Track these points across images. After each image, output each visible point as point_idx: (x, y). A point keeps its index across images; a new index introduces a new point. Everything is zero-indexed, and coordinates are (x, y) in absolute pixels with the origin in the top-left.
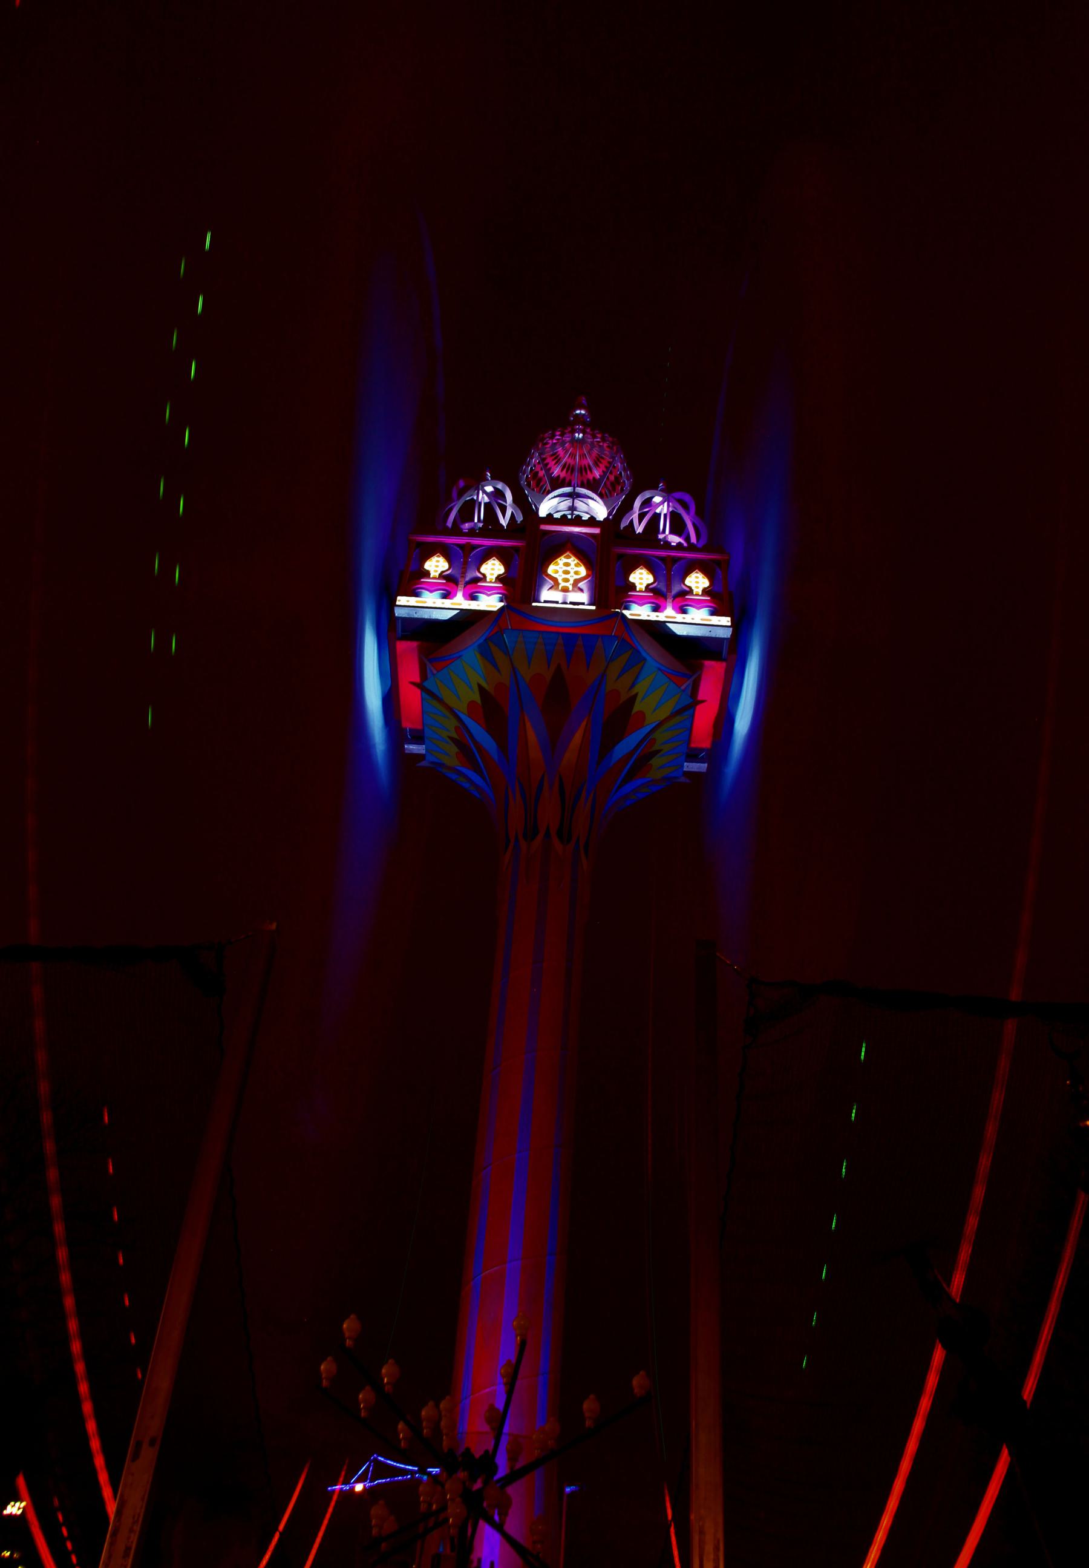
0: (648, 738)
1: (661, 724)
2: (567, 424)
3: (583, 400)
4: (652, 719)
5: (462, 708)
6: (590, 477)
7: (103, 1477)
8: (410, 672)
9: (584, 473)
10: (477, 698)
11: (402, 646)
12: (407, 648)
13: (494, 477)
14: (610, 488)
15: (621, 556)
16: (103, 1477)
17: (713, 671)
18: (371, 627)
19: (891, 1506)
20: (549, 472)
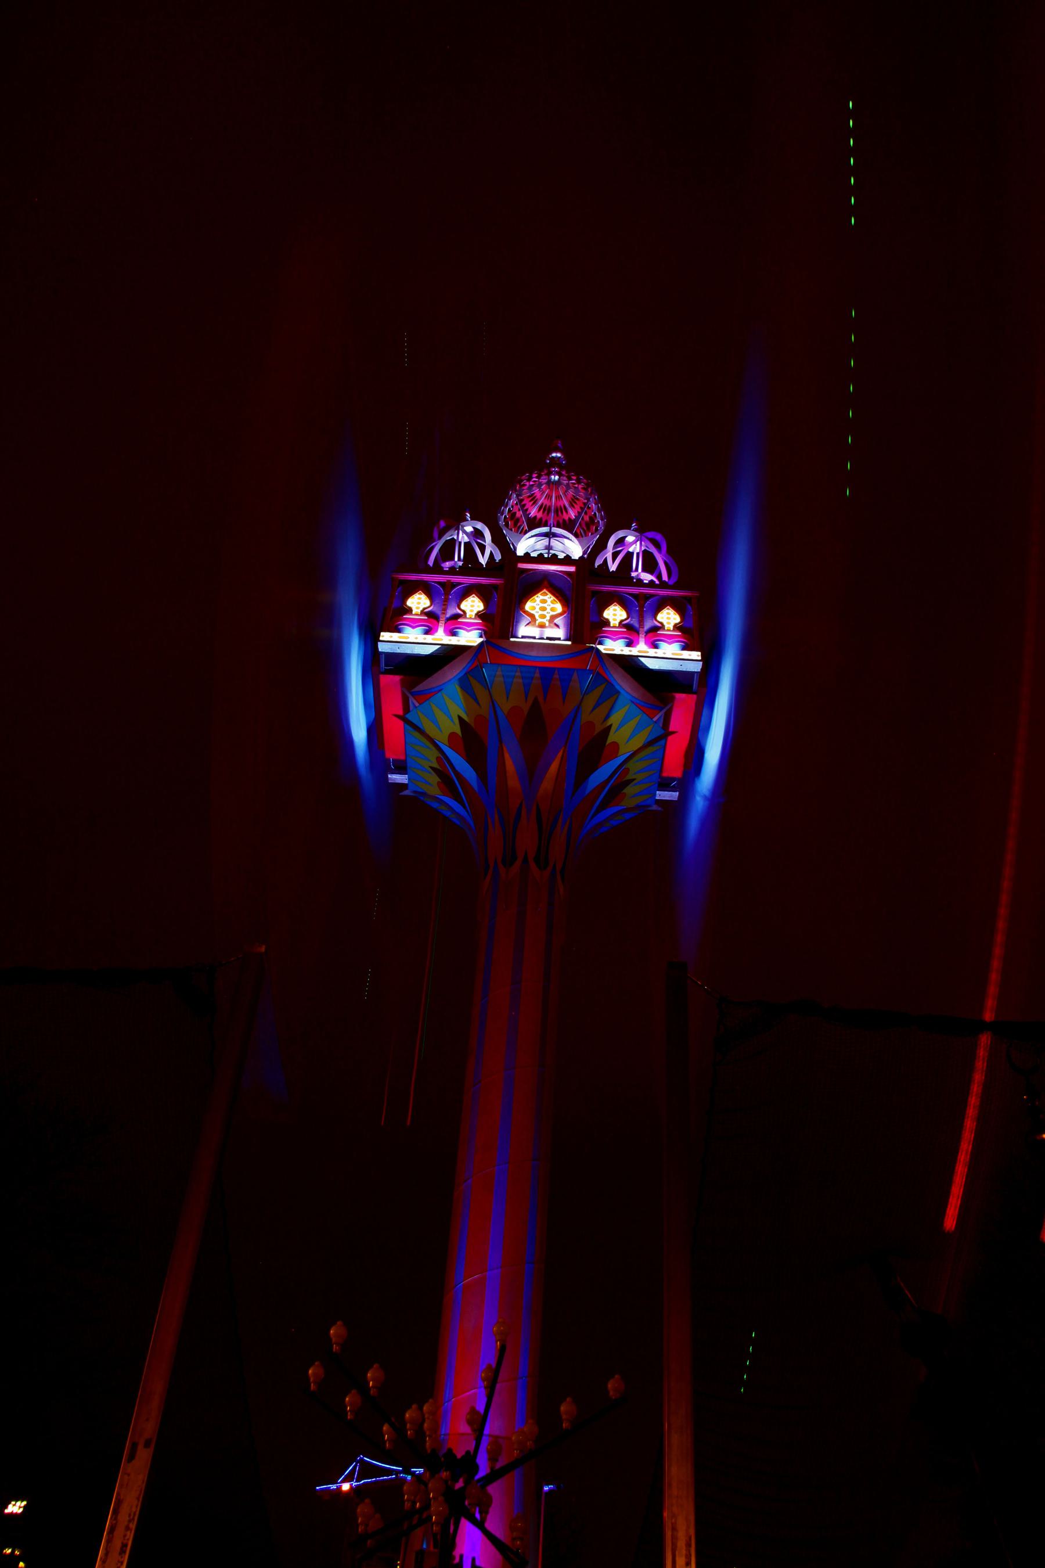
4: (625, 751)
5: (442, 739)
6: (566, 517)
8: (393, 705)
9: (560, 513)
10: (457, 729)
12: (391, 682)
15: (595, 593)
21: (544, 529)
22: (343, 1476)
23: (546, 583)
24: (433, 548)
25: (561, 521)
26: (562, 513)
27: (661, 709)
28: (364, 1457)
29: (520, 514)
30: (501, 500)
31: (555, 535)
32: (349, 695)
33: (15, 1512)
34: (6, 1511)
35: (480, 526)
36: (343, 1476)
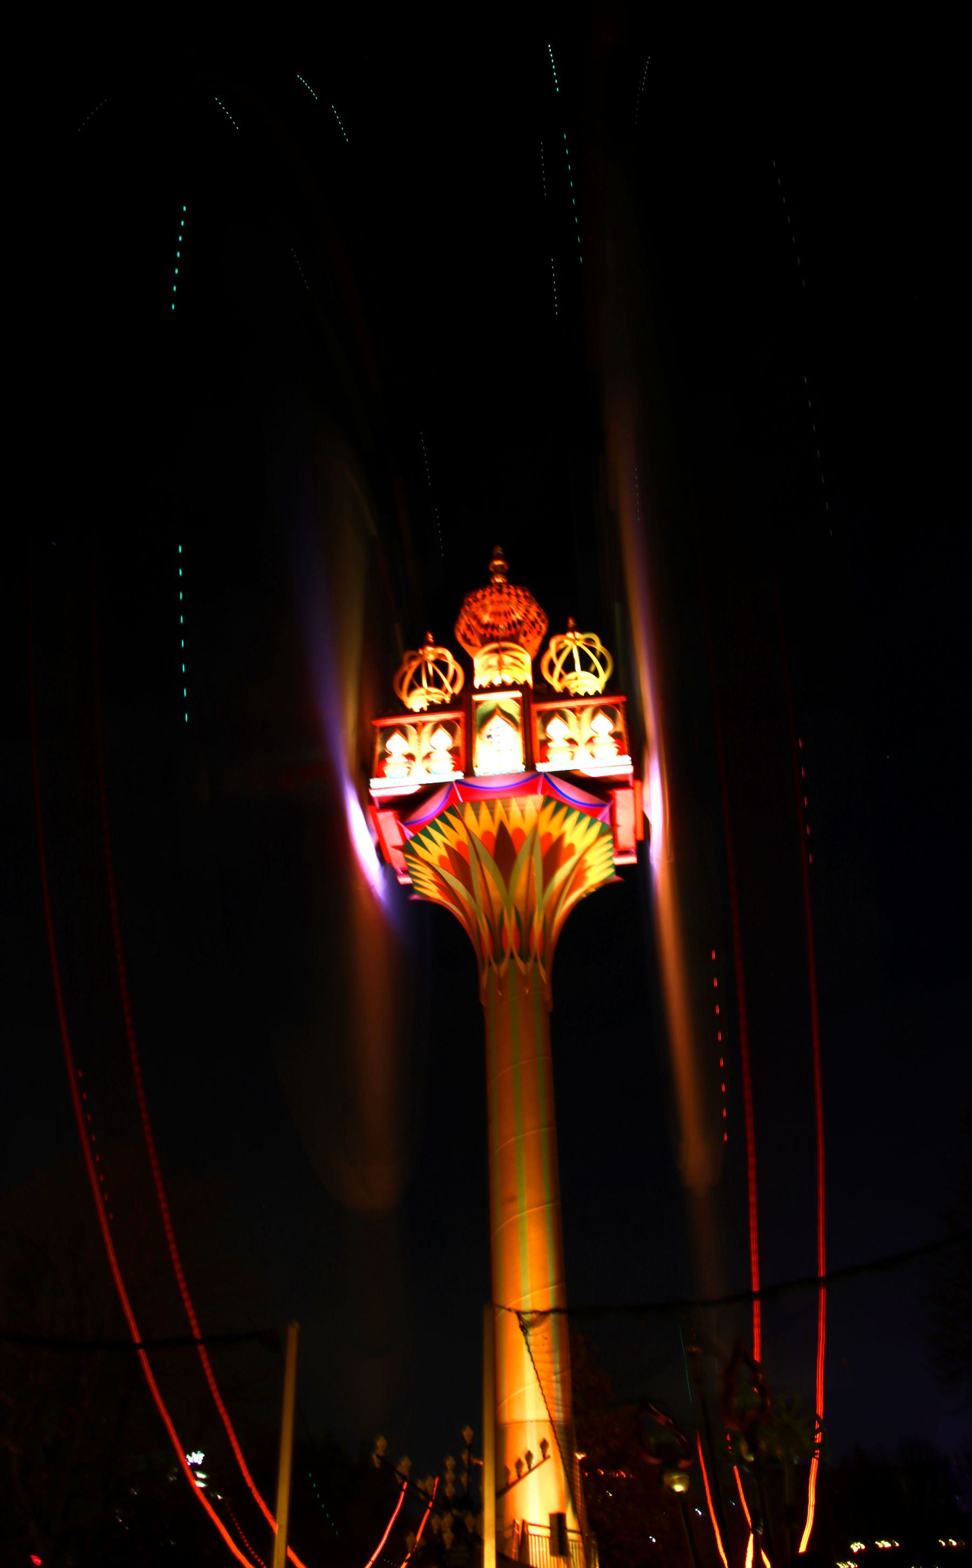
0: (581, 860)
1: (588, 849)
2: (484, 581)
3: (499, 550)
4: (579, 850)
5: (434, 861)
6: (514, 618)
7: (263, 1506)
8: (393, 836)
9: (508, 615)
10: (445, 853)
11: (382, 816)
12: (388, 820)
13: (436, 644)
14: (445, 886)
15: (540, 713)
16: (263, 1506)
17: (623, 798)
18: (381, 721)
19: (822, 1306)
20: (479, 621)
21: (494, 646)
22: (373, 1558)
23: (499, 712)
24: (406, 673)
25: (511, 622)
26: (510, 615)
27: (603, 806)
28: (406, 1492)
29: (474, 623)
30: (454, 618)
31: (505, 650)
32: (347, 807)
33: (202, 1459)
34: (32, 1556)
35: (440, 650)
36: (373, 1558)
